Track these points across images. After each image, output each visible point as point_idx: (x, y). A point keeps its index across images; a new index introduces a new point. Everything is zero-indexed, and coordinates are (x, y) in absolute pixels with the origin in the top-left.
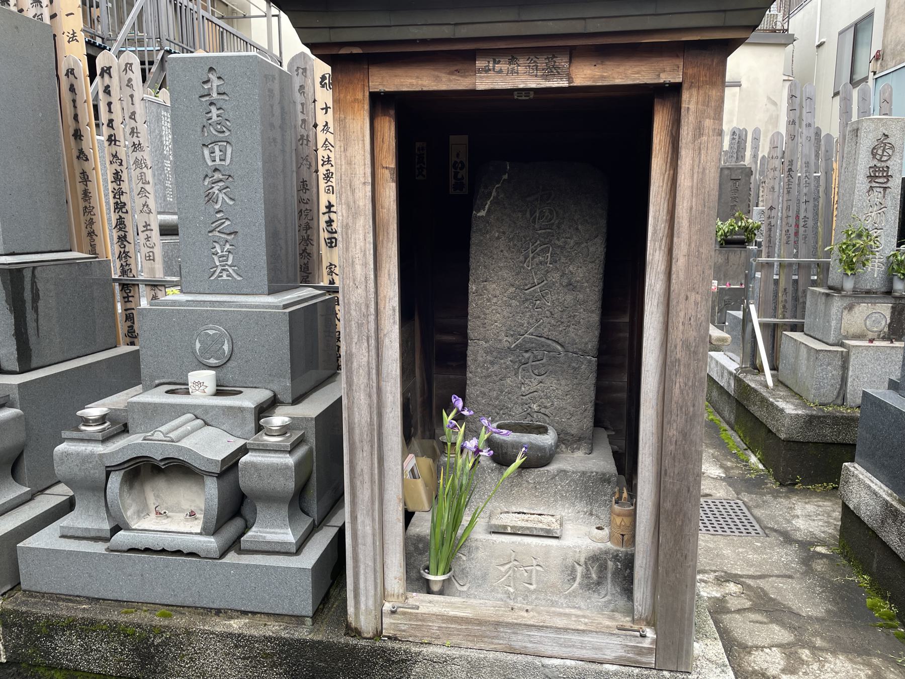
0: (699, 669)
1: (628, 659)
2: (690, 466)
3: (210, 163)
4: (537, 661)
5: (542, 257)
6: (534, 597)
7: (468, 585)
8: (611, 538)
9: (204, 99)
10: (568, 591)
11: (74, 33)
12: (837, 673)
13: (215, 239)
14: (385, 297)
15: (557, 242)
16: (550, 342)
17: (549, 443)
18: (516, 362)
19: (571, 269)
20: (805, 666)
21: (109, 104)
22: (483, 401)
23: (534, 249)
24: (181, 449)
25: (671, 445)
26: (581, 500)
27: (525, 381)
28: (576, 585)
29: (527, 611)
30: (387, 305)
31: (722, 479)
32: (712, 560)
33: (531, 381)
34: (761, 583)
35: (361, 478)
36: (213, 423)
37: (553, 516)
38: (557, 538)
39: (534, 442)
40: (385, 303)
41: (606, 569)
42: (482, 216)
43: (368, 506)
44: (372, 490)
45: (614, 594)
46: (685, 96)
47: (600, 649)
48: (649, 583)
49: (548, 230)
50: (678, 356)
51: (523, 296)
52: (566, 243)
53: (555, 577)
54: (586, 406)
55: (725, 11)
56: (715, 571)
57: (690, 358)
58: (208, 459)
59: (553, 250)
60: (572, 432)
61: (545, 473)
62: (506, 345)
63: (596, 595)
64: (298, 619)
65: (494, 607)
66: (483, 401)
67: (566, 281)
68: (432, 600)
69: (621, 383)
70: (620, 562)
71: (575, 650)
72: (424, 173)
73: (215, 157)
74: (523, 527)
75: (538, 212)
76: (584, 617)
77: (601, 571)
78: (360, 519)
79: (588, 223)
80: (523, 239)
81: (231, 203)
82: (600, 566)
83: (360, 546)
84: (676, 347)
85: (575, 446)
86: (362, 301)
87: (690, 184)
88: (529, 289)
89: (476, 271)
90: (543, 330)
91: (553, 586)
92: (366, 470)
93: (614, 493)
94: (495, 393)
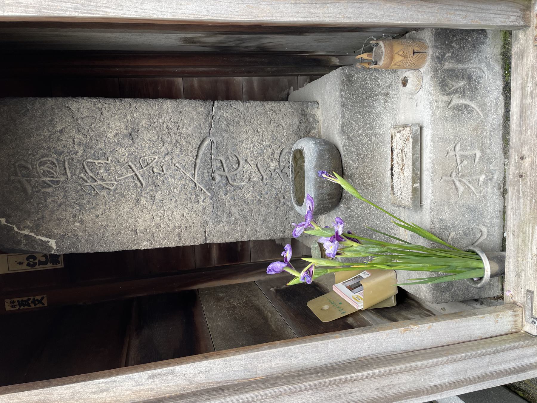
5: (100, 169)
6: (488, 151)
7: (481, 227)
8: (415, 68)
10: (480, 112)
14: (134, 392)
15: (80, 154)
16: (201, 154)
17: (313, 146)
18: (226, 189)
19: (112, 135)
22: (272, 220)
23: (91, 179)
26: (373, 106)
27: (246, 178)
28: (473, 105)
29: (522, 158)
30: (147, 387)
33: (246, 172)
35: (386, 389)
37: (392, 137)
38: (421, 129)
39: (314, 164)
40: (144, 390)
41: (454, 70)
42: (56, 243)
43: (419, 375)
44: (400, 372)
45: (479, 60)
49: (67, 165)
51: (149, 188)
52: (79, 144)
54: (268, 109)
59: (90, 158)
60: (297, 123)
61: (346, 149)
62: (208, 201)
63: (482, 81)
65: (519, 198)
66: (272, 220)
67: (127, 140)
68: (515, 273)
69: (244, 83)
70: (445, 54)
72: (39, 298)
74: (413, 169)
75: (44, 179)
77: (456, 76)
78: (437, 381)
79: (53, 118)
80: (80, 193)
82: (451, 77)
83: (468, 375)
85: (311, 119)
88: (140, 181)
89: (125, 244)
90: (187, 162)
93: (364, 69)
94: (262, 209)
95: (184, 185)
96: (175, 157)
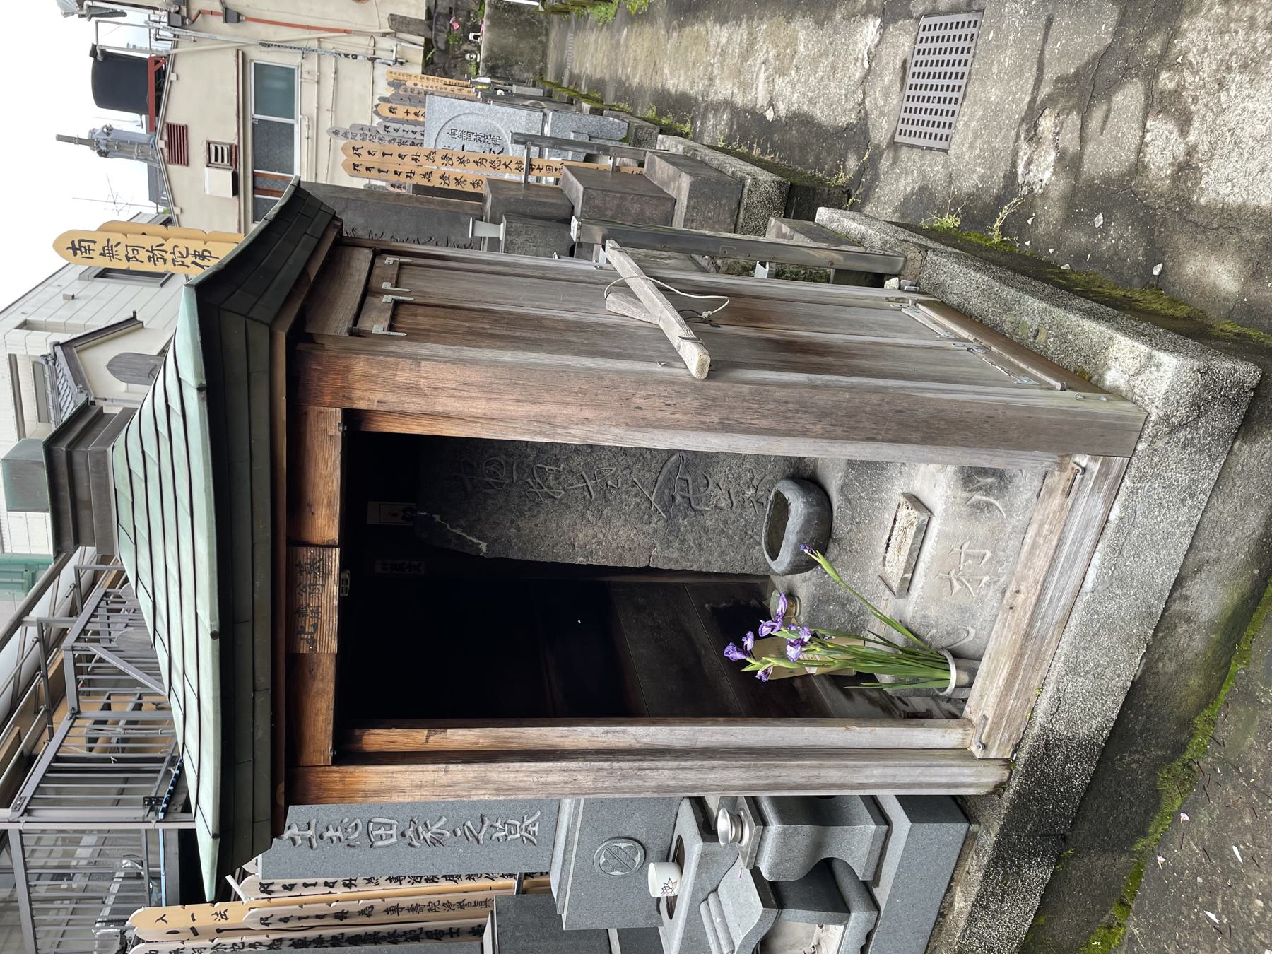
0: (1146, 398)
1: (1110, 488)
2: (868, 409)
3: (394, 840)
4: (1085, 597)
7: (969, 628)
9: (315, 845)
11: (216, 913)
12: (1206, 50)
13: (489, 836)
15: (531, 458)
16: (665, 470)
20: (1184, 93)
21: (306, 885)
24: (743, 946)
25: (834, 431)
31: (884, 27)
32: (1001, 128)
34: (1050, 74)
36: (716, 883)
39: (798, 528)
46: (361, 405)
47: (1088, 522)
48: (1016, 452)
50: (716, 420)
53: (981, 528)
55: (249, 375)
56: (1018, 136)
57: (720, 406)
58: (760, 920)
62: (661, 524)
63: (1016, 480)
64: (970, 838)
71: (1082, 550)
72: (416, 563)
73: (387, 835)
75: (488, 479)
76: (1041, 526)
81: (444, 819)
84: (704, 423)
86: (593, 775)
87: (484, 402)
91: (992, 530)
92: (804, 773)
95: (638, 504)
96: (634, 471)
